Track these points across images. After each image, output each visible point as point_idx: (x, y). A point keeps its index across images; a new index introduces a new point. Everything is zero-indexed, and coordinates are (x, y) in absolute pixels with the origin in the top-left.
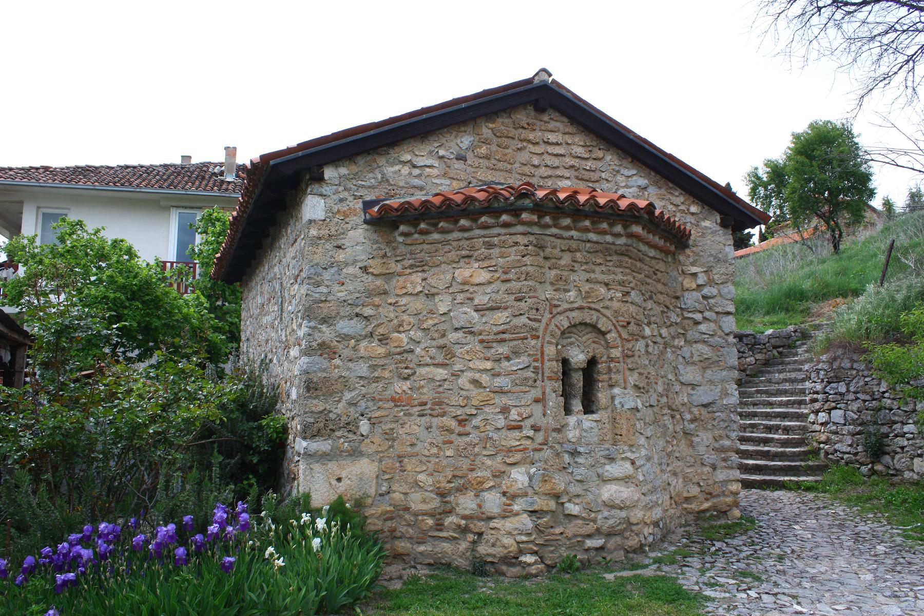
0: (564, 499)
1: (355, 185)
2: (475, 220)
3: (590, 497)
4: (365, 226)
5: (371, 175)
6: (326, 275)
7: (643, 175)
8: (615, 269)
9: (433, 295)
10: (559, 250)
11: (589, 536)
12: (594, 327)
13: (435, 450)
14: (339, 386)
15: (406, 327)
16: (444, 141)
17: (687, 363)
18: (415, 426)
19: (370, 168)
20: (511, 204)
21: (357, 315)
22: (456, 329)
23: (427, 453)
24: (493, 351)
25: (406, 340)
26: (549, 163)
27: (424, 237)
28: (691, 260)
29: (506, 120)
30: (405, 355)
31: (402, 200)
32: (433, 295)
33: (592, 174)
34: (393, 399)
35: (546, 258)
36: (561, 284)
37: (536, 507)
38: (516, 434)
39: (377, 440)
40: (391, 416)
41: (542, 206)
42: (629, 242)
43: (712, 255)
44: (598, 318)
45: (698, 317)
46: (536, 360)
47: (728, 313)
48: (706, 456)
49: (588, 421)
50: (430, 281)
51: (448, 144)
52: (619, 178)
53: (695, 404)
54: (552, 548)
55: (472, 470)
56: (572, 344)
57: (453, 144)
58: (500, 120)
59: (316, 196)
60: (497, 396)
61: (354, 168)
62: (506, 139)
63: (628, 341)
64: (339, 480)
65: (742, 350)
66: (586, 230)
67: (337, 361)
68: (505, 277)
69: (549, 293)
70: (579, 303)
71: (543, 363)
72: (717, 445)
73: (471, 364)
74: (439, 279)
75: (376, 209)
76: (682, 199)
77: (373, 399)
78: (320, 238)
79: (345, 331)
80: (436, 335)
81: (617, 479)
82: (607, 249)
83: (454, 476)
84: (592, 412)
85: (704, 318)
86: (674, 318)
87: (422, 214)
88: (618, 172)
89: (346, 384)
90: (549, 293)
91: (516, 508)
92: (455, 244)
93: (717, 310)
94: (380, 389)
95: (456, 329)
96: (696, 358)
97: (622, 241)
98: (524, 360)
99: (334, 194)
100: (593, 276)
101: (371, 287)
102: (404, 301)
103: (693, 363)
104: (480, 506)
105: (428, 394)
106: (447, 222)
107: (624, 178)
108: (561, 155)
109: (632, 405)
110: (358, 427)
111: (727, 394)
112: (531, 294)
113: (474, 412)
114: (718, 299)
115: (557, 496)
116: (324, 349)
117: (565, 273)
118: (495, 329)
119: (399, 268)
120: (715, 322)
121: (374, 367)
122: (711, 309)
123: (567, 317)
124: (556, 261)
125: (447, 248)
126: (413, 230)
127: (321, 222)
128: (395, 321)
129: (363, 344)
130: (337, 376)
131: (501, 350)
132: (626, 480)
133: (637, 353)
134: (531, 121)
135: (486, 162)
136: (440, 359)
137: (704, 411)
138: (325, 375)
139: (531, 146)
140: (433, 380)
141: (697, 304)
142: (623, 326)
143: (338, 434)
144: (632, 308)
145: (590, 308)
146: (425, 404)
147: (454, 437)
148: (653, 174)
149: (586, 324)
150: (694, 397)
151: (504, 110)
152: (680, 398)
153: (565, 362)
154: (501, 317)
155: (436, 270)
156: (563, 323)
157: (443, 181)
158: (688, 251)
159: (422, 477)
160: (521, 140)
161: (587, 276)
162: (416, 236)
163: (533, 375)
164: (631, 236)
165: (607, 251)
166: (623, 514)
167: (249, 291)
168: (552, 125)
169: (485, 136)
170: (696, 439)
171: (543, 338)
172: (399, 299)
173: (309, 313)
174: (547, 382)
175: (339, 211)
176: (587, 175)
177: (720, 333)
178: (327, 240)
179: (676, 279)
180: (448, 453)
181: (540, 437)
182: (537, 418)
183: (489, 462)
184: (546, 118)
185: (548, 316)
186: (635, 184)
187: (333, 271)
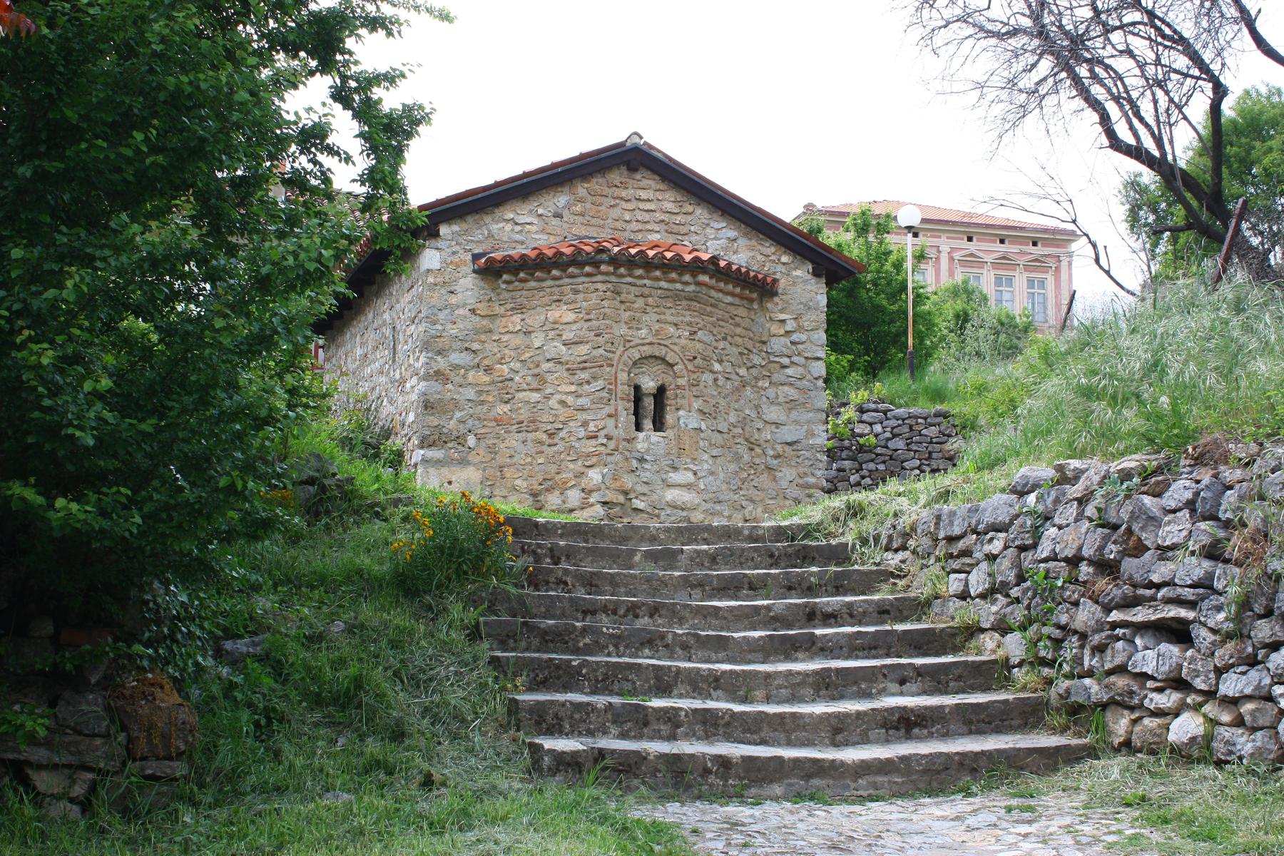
0: (632, 495)
2: (564, 271)
3: (655, 497)
4: (474, 275)
6: (441, 316)
9: (530, 332)
12: (663, 360)
13: (529, 460)
14: (451, 406)
15: (508, 360)
16: (542, 200)
17: (772, 403)
18: (514, 441)
20: (592, 258)
21: (467, 349)
22: (548, 360)
23: (522, 462)
24: (577, 377)
25: (507, 370)
26: (640, 219)
27: (523, 284)
28: (780, 307)
29: (600, 180)
30: (506, 383)
31: (506, 253)
32: (530, 332)
33: (681, 227)
34: (496, 420)
35: (622, 302)
36: (634, 324)
37: (607, 499)
38: (593, 442)
39: (482, 452)
41: (617, 259)
42: (698, 289)
43: (802, 303)
44: (667, 353)
45: (786, 361)
46: (611, 384)
47: (818, 359)
49: (656, 437)
50: (527, 321)
51: (546, 204)
52: (708, 230)
55: (558, 473)
56: (643, 373)
57: (551, 203)
58: (594, 180)
60: (579, 412)
61: (465, 226)
63: (694, 372)
64: (450, 483)
65: (947, 432)
66: (657, 279)
67: (450, 386)
68: (588, 317)
69: (623, 330)
70: (650, 339)
71: (616, 386)
72: (801, 481)
73: (559, 389)
74: (535, 319)
75: (483, 260)
76: (773, 249)
77: (479, 419)
78: (436, 285)
79: (456, 362)
80: (532, 366)
82: (676, 295)
83: (544, 479)
84: (659, 431)
85: (792, 363)
86: (757, 360)
87: (521, 265)
88: (708, 225)
89: (457, 405)
90: (623, 330)
91: (592, 500)
92: (548, 290)
94: (484, 410)
95: (548, 360)
96: (781, 399)
97: (691, 288)
98: (600, 384)
100: (663, 317)
101: (479, 326)
102: (505, 338)
103: (779, 404)
104: (564, 502)
105: (524, 414)
106: (542, 272)
107: (713, 231)
108: (652, 211)
109: (696, 425)
110: (466, 441)
111: (813, 435)
113: (561, 426)
114: (808, 345)
115: (626, 493)
116: (439, 376)
117: (638, 315)
118: (579, 359)
119: (501, 311)
120: (804, 366)
121: (480, 393)
122: (799, 354)
125: (542, 294)
126: (514, 279)
128: (498, 355)
129: (471, 373)
131: (583, 376)
132: (688, 486)
133: (702, 384)
134: (624, 180)
135: (581, 219)
136: (535, 385)
137: (787, 448)
139: (623, 203)
140: (528, 402)
142: (689, 360)
143: (450, 445)
144: (698, 345)
145: (659, 344)
146: (522, 422)
147: (544, 448)
148: (743, 226)
149: (656, 357)
150: (778, 435)
151: (599, 171)
152: (763, 435)
153: (637, 388)
154: (583, 349)
155: (533, 312)
157: (541, 236)
158: (776, 299)
159: (518, 482)
161: (658, 317)
162: (517, 283)
164: (698, 284)
165: (677, 297)
166: (684, 514)
167: (338, 347)
168: (645, 182)
169: (580, 195)
170: (779, 474)
172: (502, 336)
173: (426, 346)
174: (620, 402)
175: (451, 262)
176: (676, 229)
177: (809, 377)
178: (442, 286)
179: (763, 326)
180: (540, 461)
181: (612, 444)
183: (571, 466)
184: (638, 176)
185: (621, 349)
187: (446, 312)
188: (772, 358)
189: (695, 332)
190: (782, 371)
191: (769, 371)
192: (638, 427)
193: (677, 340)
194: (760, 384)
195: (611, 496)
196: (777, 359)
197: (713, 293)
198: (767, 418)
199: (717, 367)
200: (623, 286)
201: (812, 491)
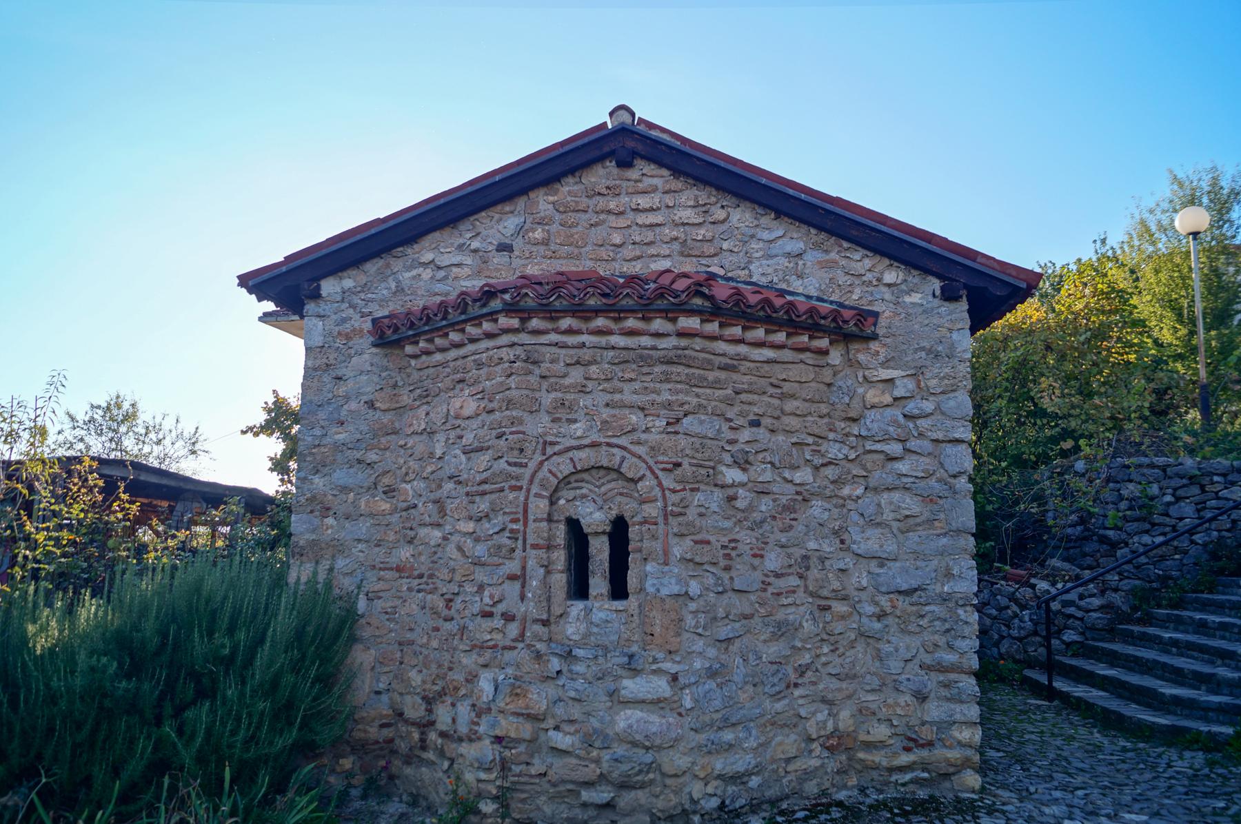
1: (363, 300)
4: (374, 350)
5: (383, 285)
7: (795, 235)
8: (658, 385)
10: (562, 364)
11: (589, 784)
19: (381, 276)
21: (359, 461)
26: (638, 239)
28: (881, 358)
33: (706, 245)
34: (398, 569)
40: (393, 591)
42: (684, 342)
43: (923, 349)
44: (623, 459)
45: (895, 448)
48: (904, 676)
53: (883, 589)
54: (524, 796)
56: (584, 496)
59: (313, 318)
61: (363, 279)
62: (573, 215)
63: (674, 491)
67: (330, 521)
70: (595, 437)
71: (525, 524)
72: (928, 659)
76: (868, 263)
79: (341, 482)
81: (643, 702)
82: (641, 357)
86: (834, 451)
88: (752, 236)
93: (935, 436)
99: (336, 313)
100: (617, 397)
109: (676, 589)
111: (949, 575)
112: (514, 429)
118: (478, 478)
123: (571, 459)
124: (558, 380)
127: (319, 350)
130: (329, 538)
135: (542, 248)
137: (902, 603)
138: (314, 537)
139: (612, 218)
141: (891, 429)
145: (608, 444)
148: (813, 231)
150: (881, 579)
153: (574, 525)
154: (483, 459)
156: (563, 467)
160: (597, 213)
161: (608, 397)
163: (508, 542)
164: (681, 334)
166: (648, 758)
171: (528, 491)
174: (533, 553)
175: (339, 333)
181: (513, 629)
182: (511, 603)
184: (633, 174)
186: (781, 252)
188: (869, 446)
189: (678, 420)
190: (889, 465)
191: (864, 468)
192: (579, 589)
193: (644, 436)
194: (846, 491)
195: (508, 726)
196: (878, 447)
197: (721, 346)
198: (861, 548)
199: (733, 475)
200: (544, 349)
201: (953, 676)
